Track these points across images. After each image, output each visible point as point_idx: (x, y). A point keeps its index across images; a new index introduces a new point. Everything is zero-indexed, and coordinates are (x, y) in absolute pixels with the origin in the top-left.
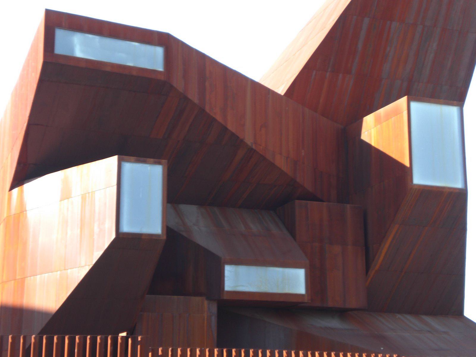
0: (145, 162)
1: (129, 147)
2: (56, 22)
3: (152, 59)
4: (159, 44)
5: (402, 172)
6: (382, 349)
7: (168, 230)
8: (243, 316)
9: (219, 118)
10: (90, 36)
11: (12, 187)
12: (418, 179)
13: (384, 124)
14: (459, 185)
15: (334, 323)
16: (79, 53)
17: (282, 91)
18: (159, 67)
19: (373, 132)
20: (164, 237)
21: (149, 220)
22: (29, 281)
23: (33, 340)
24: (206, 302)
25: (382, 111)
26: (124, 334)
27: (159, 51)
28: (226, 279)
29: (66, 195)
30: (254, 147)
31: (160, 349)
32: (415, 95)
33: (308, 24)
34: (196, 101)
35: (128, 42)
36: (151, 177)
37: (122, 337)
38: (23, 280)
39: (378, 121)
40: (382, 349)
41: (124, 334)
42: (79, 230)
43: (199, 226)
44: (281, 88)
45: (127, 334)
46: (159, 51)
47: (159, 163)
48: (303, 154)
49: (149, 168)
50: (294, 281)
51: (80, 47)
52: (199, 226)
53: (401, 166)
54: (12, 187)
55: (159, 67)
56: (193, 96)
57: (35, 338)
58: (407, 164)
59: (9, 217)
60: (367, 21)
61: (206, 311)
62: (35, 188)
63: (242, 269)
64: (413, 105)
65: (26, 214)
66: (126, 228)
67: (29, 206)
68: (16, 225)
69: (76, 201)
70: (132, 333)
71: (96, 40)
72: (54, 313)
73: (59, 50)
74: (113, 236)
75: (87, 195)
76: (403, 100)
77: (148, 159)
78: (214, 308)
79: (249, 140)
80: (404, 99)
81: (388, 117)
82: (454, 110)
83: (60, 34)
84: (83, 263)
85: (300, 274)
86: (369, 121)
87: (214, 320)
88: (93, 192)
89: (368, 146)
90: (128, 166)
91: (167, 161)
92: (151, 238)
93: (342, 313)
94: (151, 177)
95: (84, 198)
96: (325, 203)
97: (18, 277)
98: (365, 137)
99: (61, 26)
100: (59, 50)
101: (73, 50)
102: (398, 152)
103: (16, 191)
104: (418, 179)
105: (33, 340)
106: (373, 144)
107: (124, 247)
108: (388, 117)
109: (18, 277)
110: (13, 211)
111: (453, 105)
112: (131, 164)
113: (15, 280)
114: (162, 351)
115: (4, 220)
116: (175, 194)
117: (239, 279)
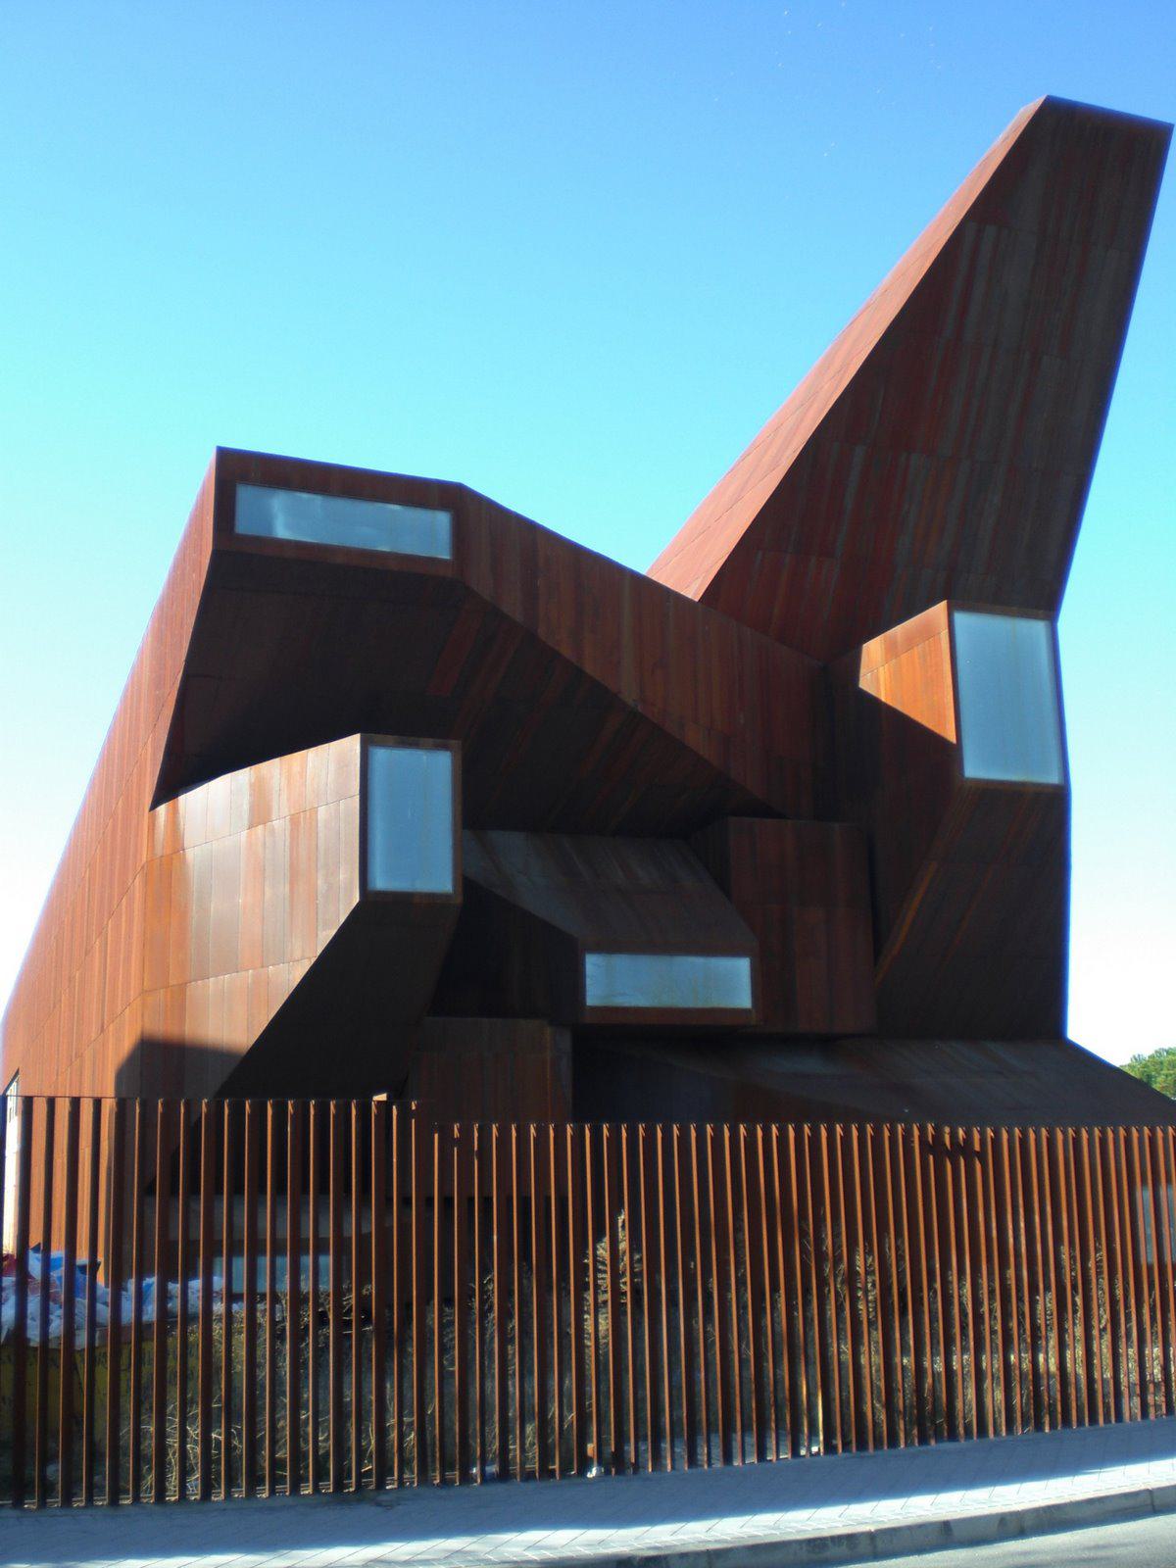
0: (416, 745)
1: (381, 720)
2: (237, 472)
3: (428, 536)
4: (442, 506)
5: (941, 755)
6: (907, 1111)
7: (467, 883)
8: (630, 1065)
9: (566, 651)
10: (305, 496)
11: (155, 805)
12: (974, 768)
13: (904, 657)
14: (1054, 779)
15: (811, 1064)
16: (282, 531)
17: (695, 594)
18: (445, 555)
19: (883, 673)
20: (459, 900)
21: (430, 869)
22: (195, 989)
23: (204, 1109)
24: (549, 1031)
25: (898, 630)
26: (383, 1097)
27: (442, 520)
28: (588, 981)
29: (260, 814)
30: (640, 709)
31: (456, 1127)
32: (961, 600)
33: (743, 458)
34: (518, 616)
35: (379, 505)
36: (429, 772)
37: (379, 1102)
38: (182, 987)
39: (892, 651)
40: (907, 1111)
41: (383, 1097)
42: (285, 889)
43: (531, 876)
44: (693, 589)
45: (388, 1097)
46: (442, 520)
47: (445, 747)
48: (742, 721)
49: (425, 757)
50: (728, 982)
51: (285, 519)
52: (531, 876)
53: (939, 741)
54: (155, 805)
55: (445, 555)
56: (513, 606)
57: (207, 1105)
58: (952, 738)
59: (150, 862)
60: (859, 454)
61: (548, 1048)
62: (217, 801)
63: (622, 962)
64: (960, 618)
65: (184, 855)
66: (380, 882)
67: (189, 838)
68: (166, 874)
69: (280, 824)
70: (398, 1095)
71: (314, 503)
72: (13, 1318)
73: (244, 525)
74: (356, 899)
75: (302, 815)
76: (940, 609)
77: (422, 740)
78: (566, 1042)
79: (629, 694)
80: (941, 607)
81: (910, 642)
82: (1039, 627)
83: (246, 495)
84: (297, 954)
85: (740, 969)
86: (873, 649)
87: (565, 1066)
88: (314, 810)
89: (873, 702)
90: (381, 755)
91: (460, 742)
92: (430, 903)
93: (826, 1043)
94: (429, 772)
95: (294, 821)
96: (789, 821)
97: (172, 982)
98: (866, 683)
99: (246, 480)
100: (244, 525)
101: (270, 526)
102: (934, 714)
103: (162, 809)
104: (974, 768)
105: (204, 1109)
106: (883, 700)
107: (377, 920)
108: (910, 642)
109: (172, 982)
110: (159, 851)
111: (1036, 617)
112: (389, 751)
113: (167, 987)
114: (459, 1130)
115: (143, 867)
116: (478, 811)
117: (614, 981)
